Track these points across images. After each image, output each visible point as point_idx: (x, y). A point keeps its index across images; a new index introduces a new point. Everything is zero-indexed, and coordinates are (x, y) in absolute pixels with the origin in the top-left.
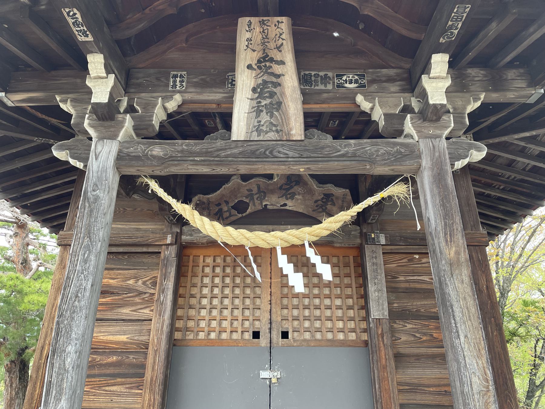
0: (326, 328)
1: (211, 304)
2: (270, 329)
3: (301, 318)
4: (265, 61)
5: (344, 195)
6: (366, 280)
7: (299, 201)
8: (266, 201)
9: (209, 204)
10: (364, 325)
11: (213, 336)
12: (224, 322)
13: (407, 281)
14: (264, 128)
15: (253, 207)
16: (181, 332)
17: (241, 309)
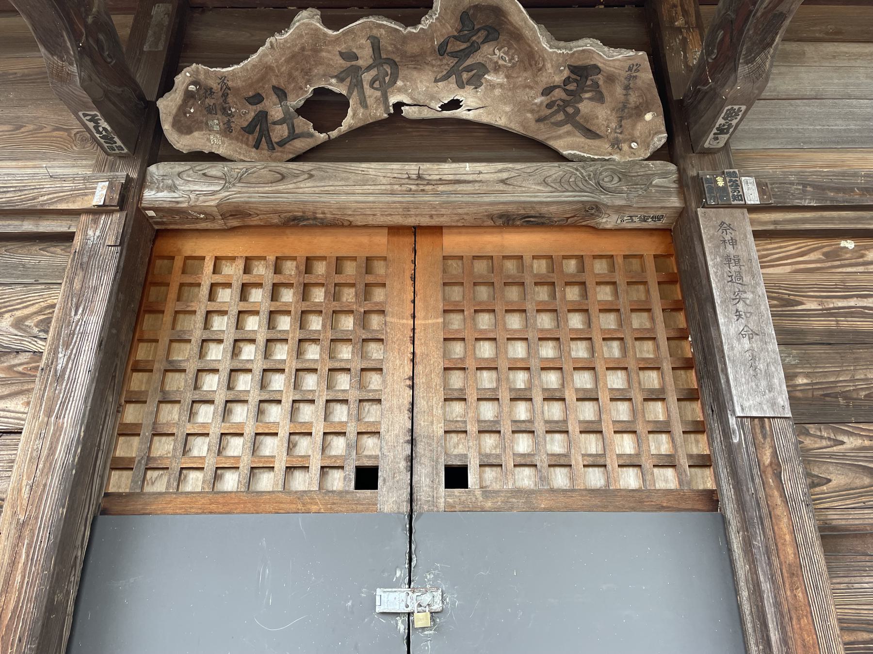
0: (583, 455)
1: (229, 388)
2: (411, 459)
3: (506, 428)
5: (630, 69)
6: (709, 308)
7: (497, 92)
8: (400, 90)
9: (225, 96)
11: (231, 482)
12: (269, 441)
13: (829, 313)
15: (361, 111)
16: (130, 473)
17: (321, 403)
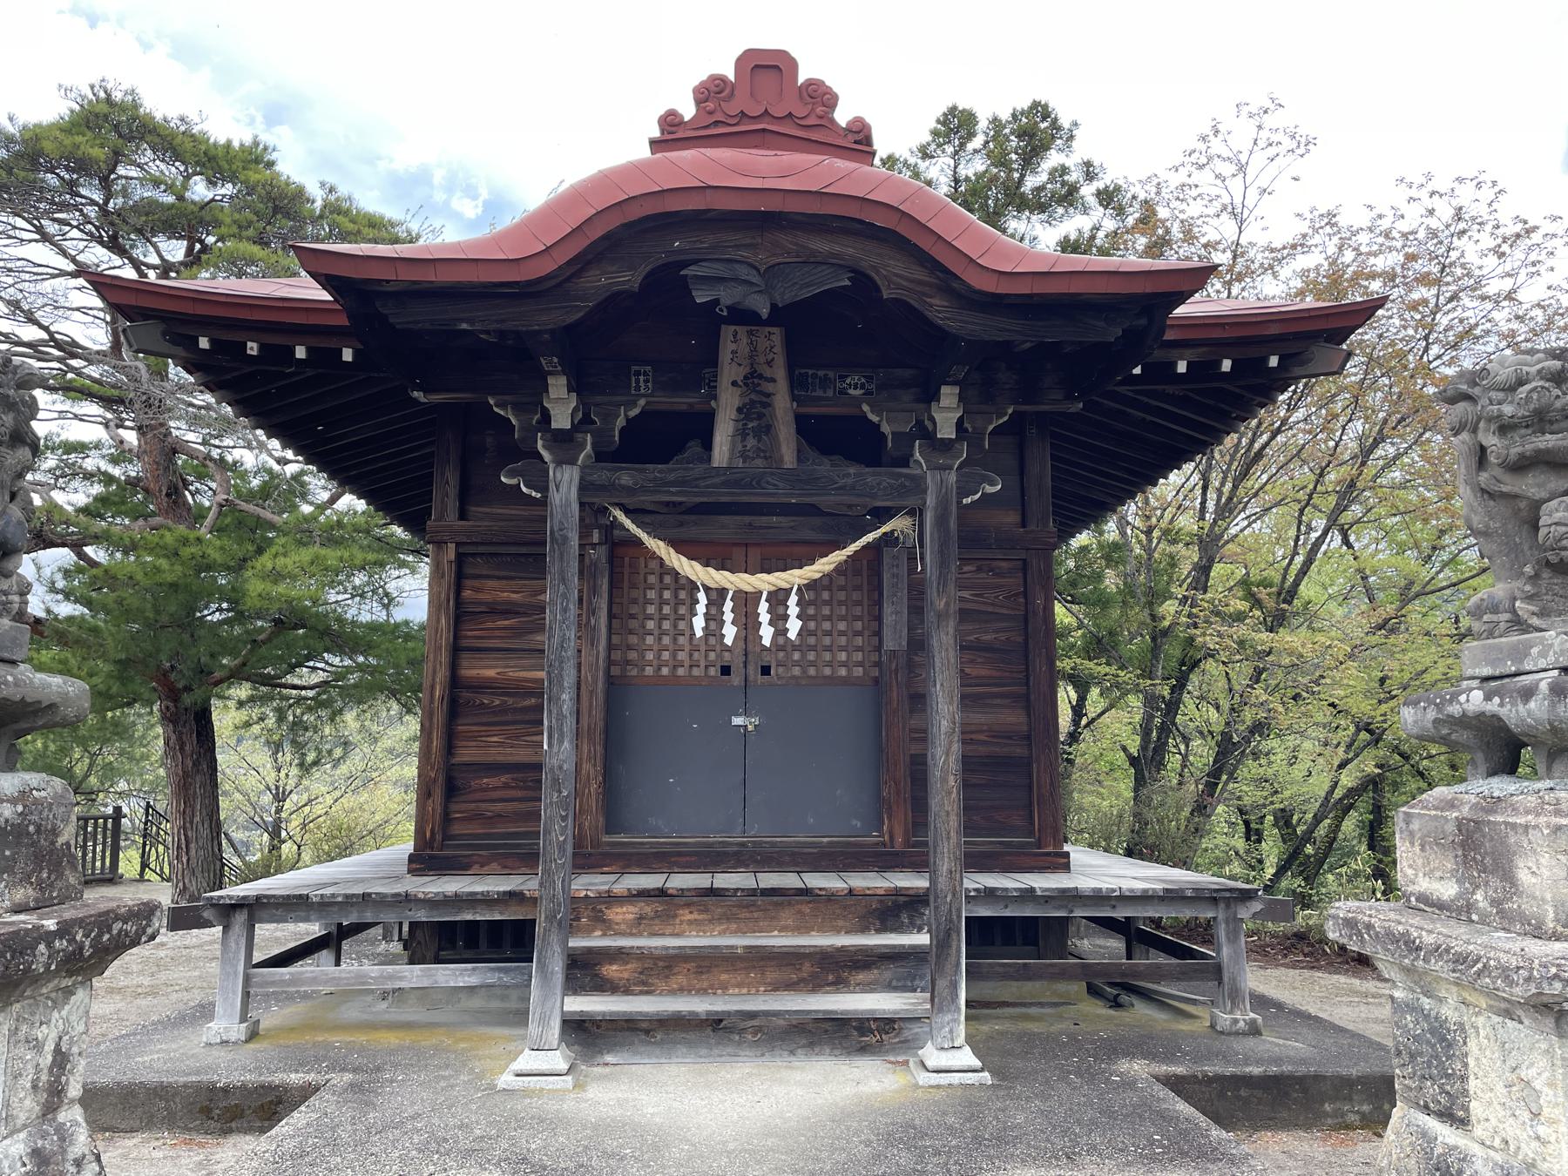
2: (745, 663)
4: (753, 377)
10: (874, 657)
14: (750, 454)
